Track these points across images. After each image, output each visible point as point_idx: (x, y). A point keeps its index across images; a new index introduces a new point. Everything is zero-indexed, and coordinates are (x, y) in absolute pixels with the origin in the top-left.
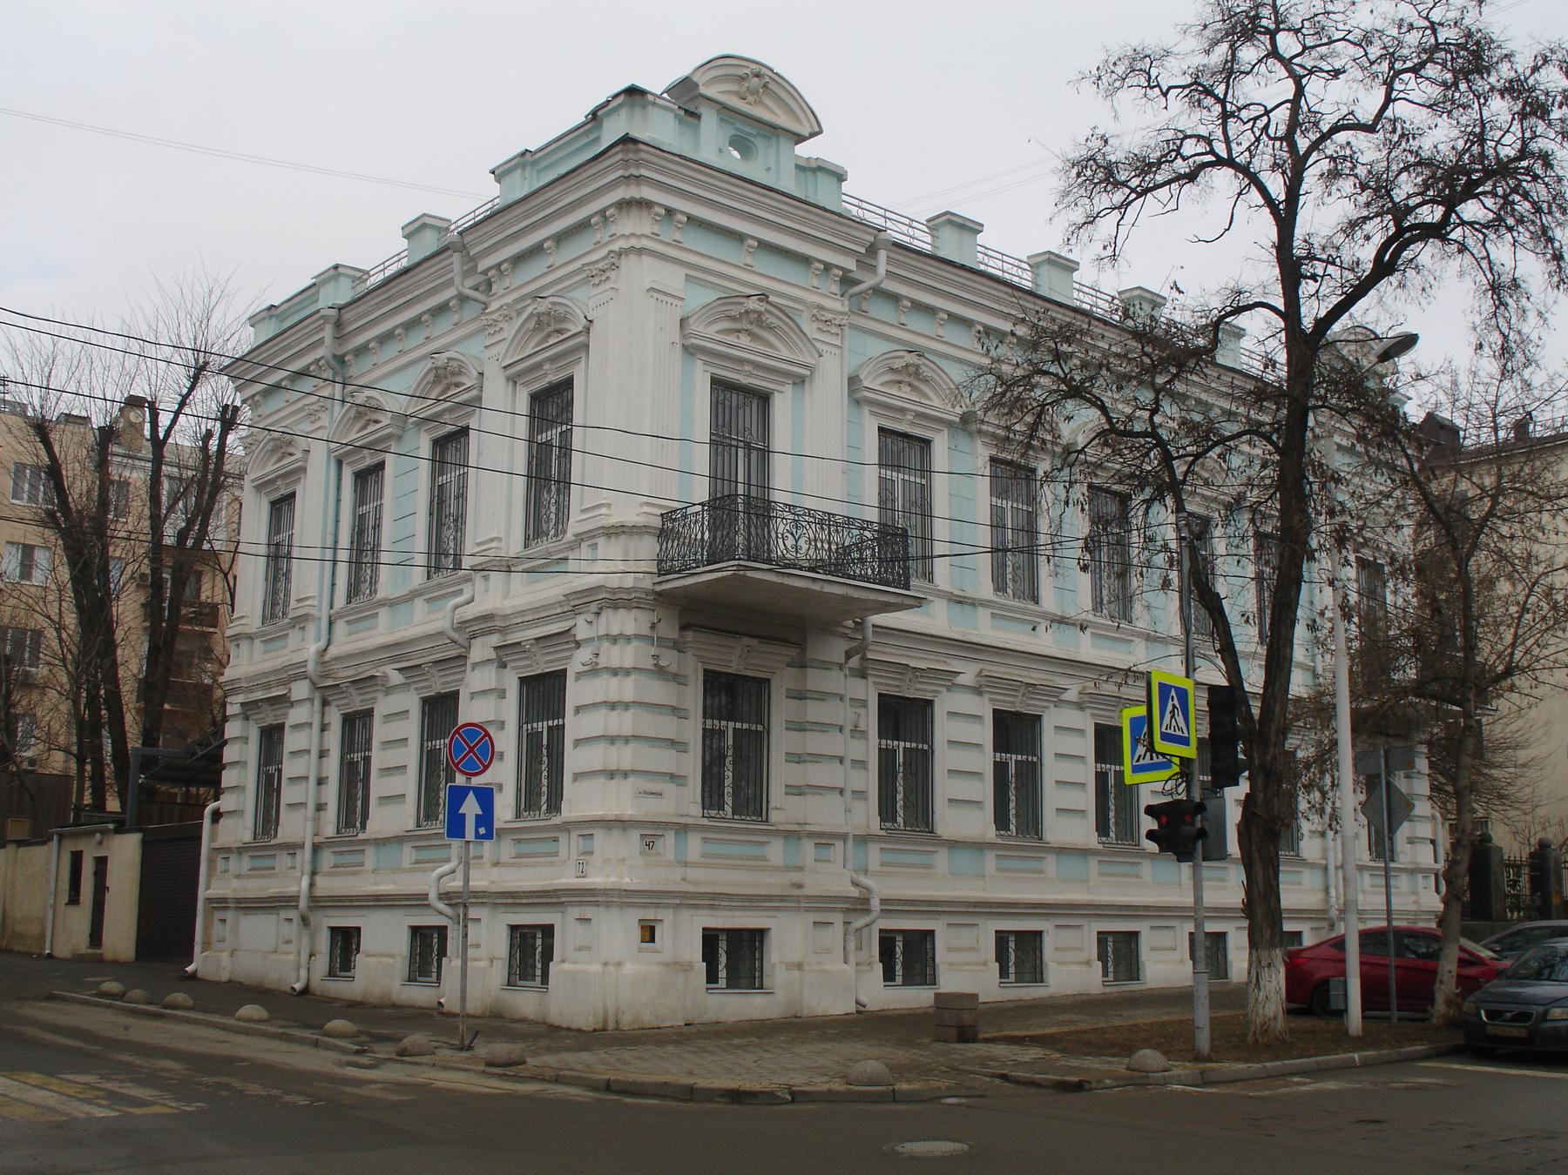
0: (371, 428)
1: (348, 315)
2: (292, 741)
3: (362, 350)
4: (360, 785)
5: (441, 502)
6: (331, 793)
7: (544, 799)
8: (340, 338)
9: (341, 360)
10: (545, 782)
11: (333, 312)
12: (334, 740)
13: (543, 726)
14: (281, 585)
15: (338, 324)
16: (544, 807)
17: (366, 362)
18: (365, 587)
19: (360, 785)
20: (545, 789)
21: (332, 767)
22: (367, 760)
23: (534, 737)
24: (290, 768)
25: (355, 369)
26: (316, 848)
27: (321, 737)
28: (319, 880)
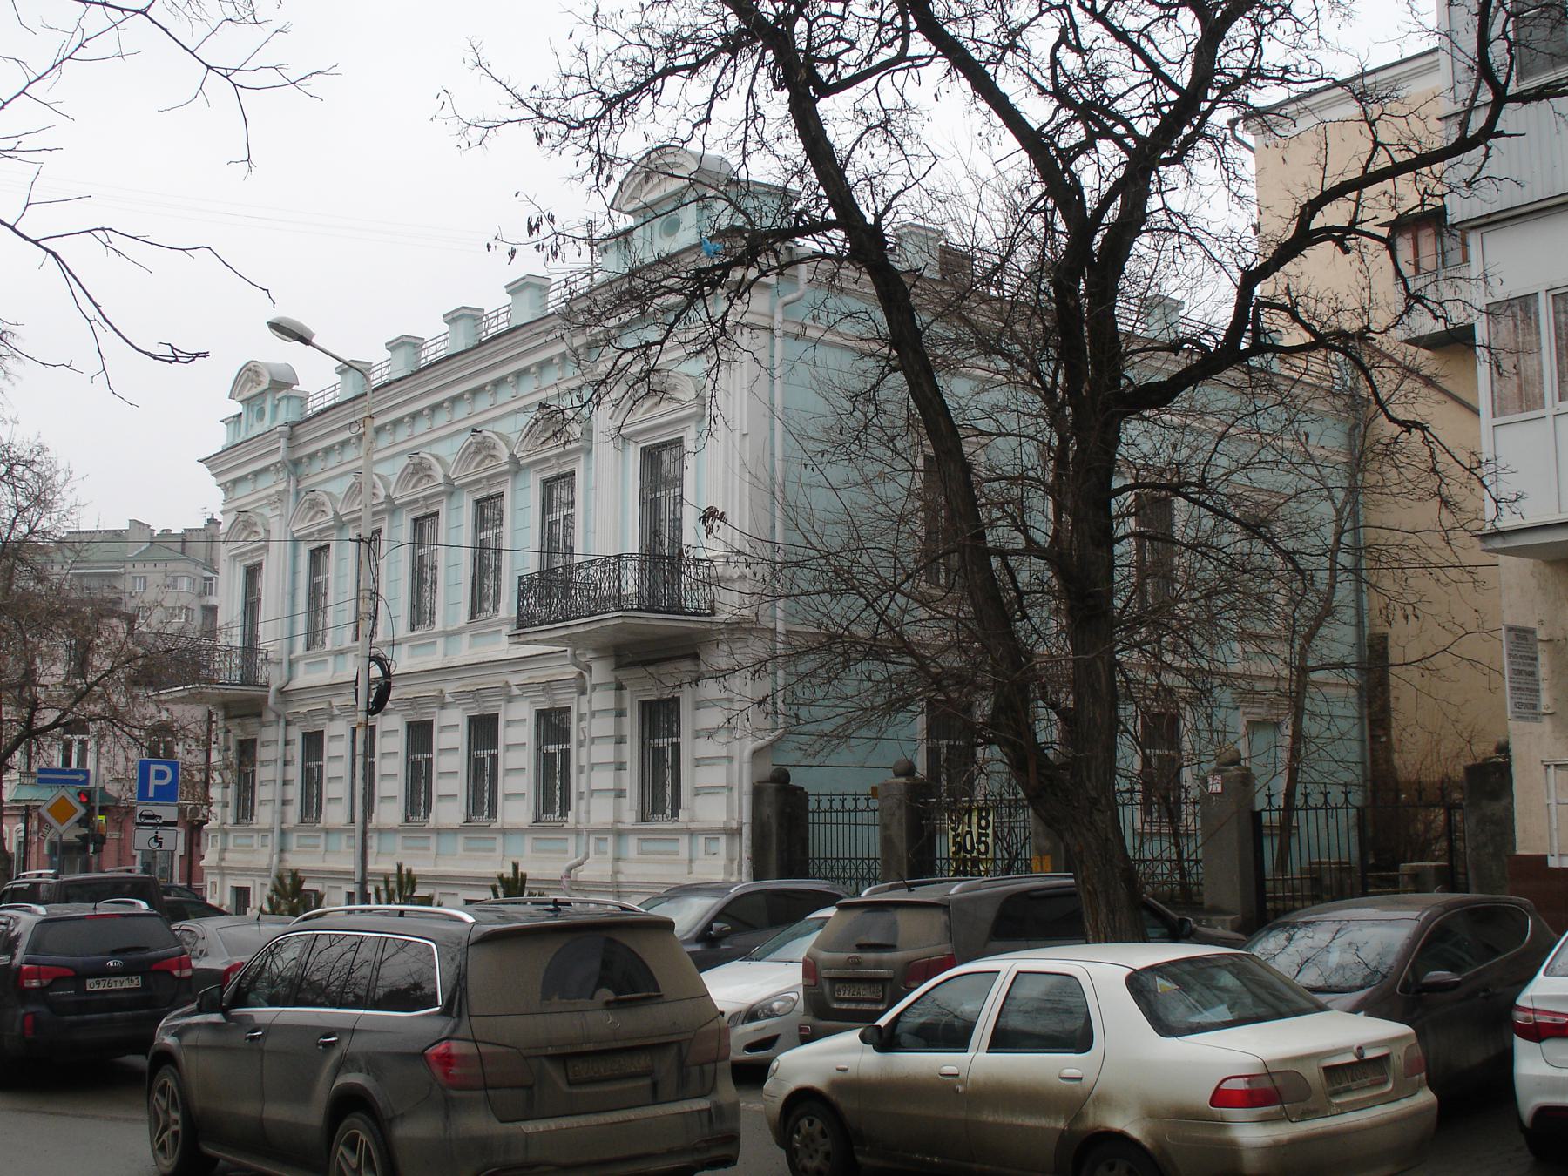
0: (487, 463)
1: (300, 430)
2: (263, 754)
3: (312, 456)
4: (669, 772)
5: (420, 571)
6: (294, 793)
7: (558, 806)
8: (292, 448)
9: (296, 463)
10: (558, 793)
11: (286, 429)
12: (297, 751)
13: (483, 753)
14: (489, 583)
15: (291, 438)
16: (486, 813)
17: (318, 465)
18: (488, 605)
19: (669, 772)
20: (558, 799)
21: (295, 772)
22: (676, 748)
23: (549, 757)
24: (263, 773)
25: (302, 469)
26: (283, 833)
27: (285, 750)
28: (287, 856)
